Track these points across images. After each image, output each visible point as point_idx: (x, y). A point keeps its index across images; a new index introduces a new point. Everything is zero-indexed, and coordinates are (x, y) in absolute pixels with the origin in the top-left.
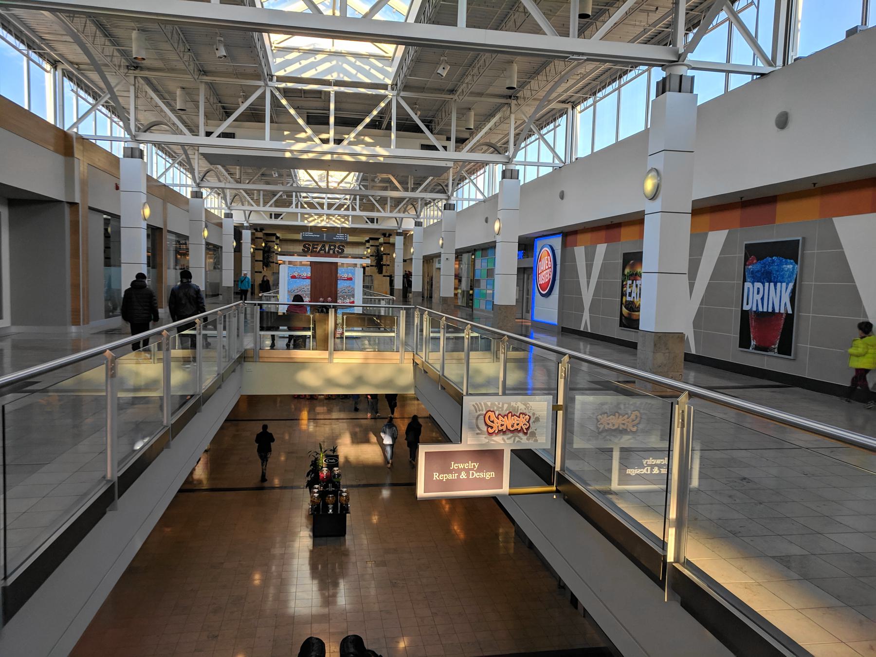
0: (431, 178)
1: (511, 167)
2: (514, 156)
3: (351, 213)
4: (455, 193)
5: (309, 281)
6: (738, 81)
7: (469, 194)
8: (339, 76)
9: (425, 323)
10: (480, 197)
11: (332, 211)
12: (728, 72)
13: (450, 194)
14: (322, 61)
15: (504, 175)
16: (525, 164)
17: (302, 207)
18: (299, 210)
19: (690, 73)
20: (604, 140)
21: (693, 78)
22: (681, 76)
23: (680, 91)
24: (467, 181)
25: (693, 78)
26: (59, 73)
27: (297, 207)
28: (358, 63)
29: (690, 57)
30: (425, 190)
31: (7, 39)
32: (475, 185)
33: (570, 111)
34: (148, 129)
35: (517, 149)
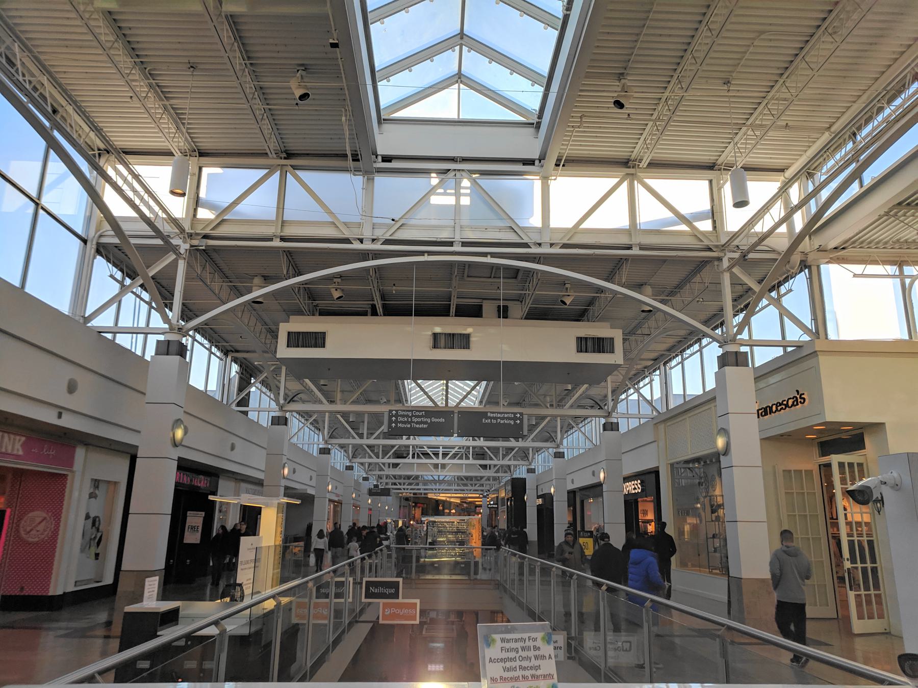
0: (586, 386)
2: (615, 407)
3: (464, 461)
4: (565, 441)
6: (789, 349)
7: (574, 443)
9: (601, 604)
11: (446, 461)
13: (530, 458)
15: (723, 361)
17: (419, 457)
18: (416, 461)
26: (229, 359)
27: (413, 457)
30: (533, 440)
33: (662, 368)
34: (292, 400)
35: (616, 401)
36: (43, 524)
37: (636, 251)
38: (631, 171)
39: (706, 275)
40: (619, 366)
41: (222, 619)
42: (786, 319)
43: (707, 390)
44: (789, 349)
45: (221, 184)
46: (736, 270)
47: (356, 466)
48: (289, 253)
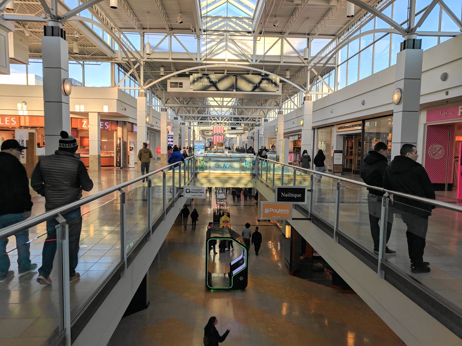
1: (281, 110)
5: (7, 252)
8: (227, 28)
10: (296, 107)
12: (439, 36)
14: (210, 21)
15: (404, 46)
16: (285, 109)
19: (418, 38)
20: (353, 80)
21: (421, 40)
22: (414, 40)
23: (413, 48)
24: (289, 99)
25: (421, 40)
28: (237, 22)
29: (418, 29)
31: (178, 181)
32: (294, 102)
35: (282, 104)
36: (441, 151)
37: (282, 64)
38: (282, 35)
39: (300, 74)
40: (280, 96)
41: (122, 187)
42: (185, 52)
43: (375, 72)
44: (443, 39)
45: (153, 39)
46: (313, 70)
47: (179, 118)
48: (174, 63)
